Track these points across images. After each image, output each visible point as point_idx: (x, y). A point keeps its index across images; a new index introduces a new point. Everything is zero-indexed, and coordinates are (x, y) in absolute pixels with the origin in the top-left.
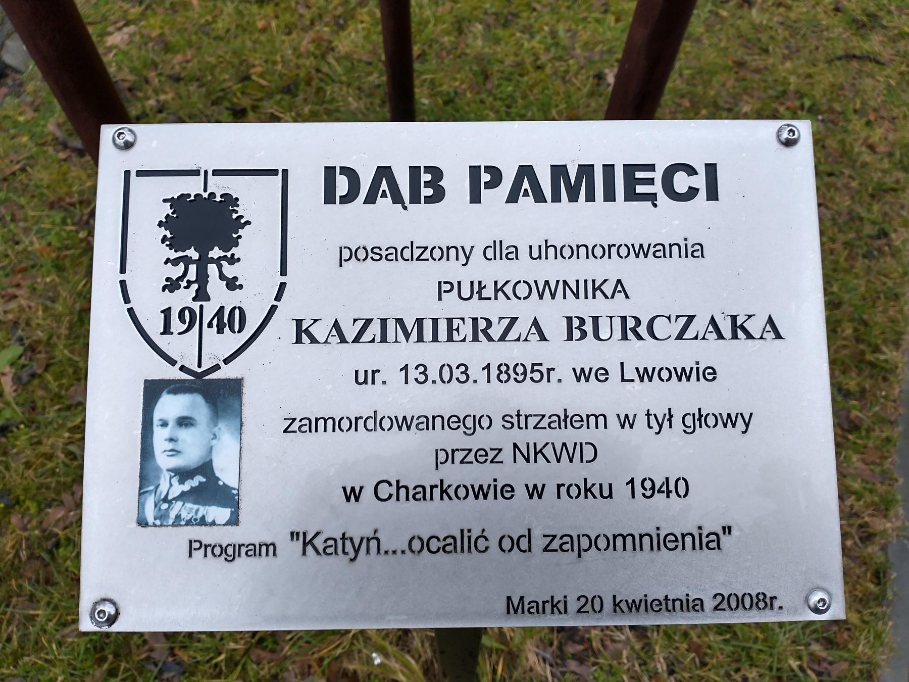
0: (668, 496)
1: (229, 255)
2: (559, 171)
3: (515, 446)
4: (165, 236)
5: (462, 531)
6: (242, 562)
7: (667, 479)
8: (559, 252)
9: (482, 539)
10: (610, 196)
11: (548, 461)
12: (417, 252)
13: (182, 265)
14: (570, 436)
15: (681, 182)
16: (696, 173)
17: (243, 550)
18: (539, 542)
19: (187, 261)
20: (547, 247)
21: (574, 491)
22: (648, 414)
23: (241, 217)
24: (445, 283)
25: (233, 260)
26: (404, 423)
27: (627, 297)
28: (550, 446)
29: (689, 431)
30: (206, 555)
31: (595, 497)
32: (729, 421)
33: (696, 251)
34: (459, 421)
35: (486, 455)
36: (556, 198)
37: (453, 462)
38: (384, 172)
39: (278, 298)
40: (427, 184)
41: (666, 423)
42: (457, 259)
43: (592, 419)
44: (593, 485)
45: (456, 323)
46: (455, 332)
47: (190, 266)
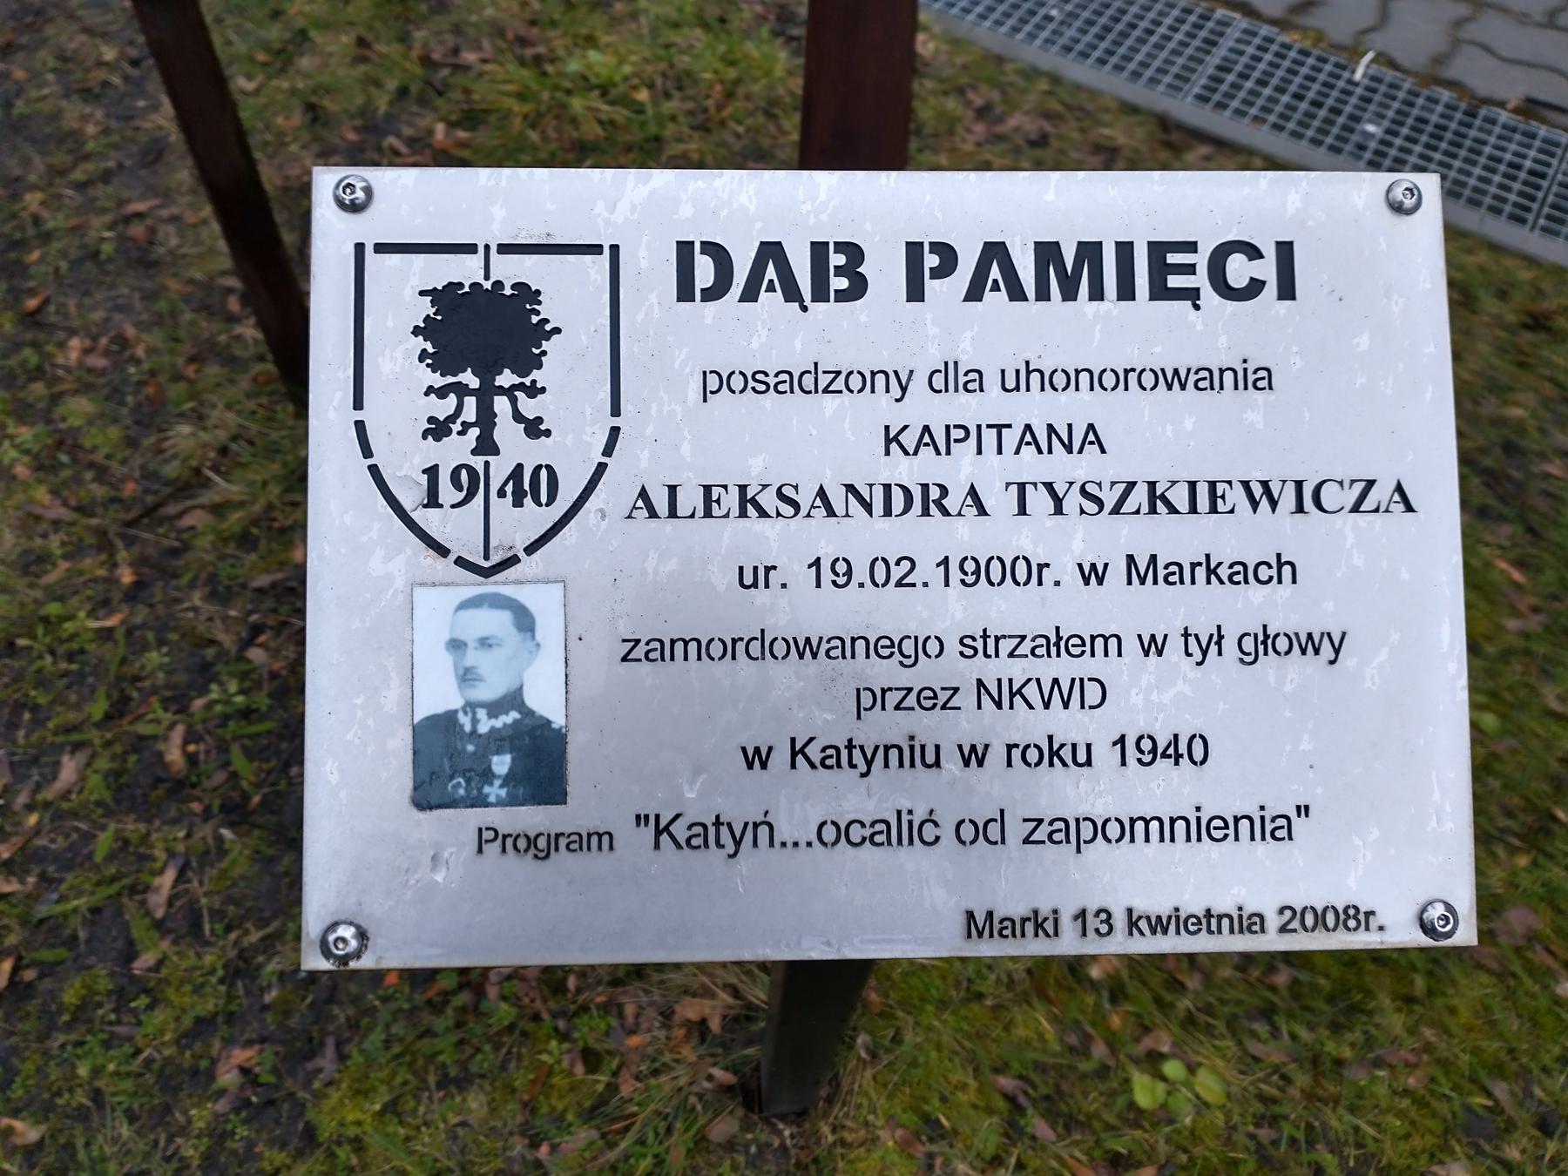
0: (1177, 763)
1: (527, 381)
2: (1047, 253)
3: (980, 683)
4: (424, 351)
5: (899, 813)
6: (562, 858)
7: (1176, 736)
8: (1048, 382)
9: (928, 826)
10: (1126, 292)
11: (1031, 707)
12: (824, 380)
13: (452, 399)
14: (1063, 668)
15: (1238, 270)
16: (1261, 256)
17: (563, 842)
18: (1016, 831)
19: (461, 390)
20: (1029, 373)
21: (1033, 755)
22: (1186, 635)
23: (546, 321)
24: (956, 427)
25: (534, 391)
26: (807, 648)
27: (1103, 451)
28: (1033, 684)
29: (1249, 659)
30: (504, 850)
31: (1065, 764)
32: (1309, 644)
33: (1258, 379)
34: (892, 646)
35: (935, 697)
36: (1043, 294)
37: (883, 708)
38: (771, 252)
39: (608, 451)
40: (839, 271)
41: (1213, 648)
42: (888, 391)
43: (1099, 642)
44: (1062, 746)
45: (1220, 489)
46: (1219, 501)
47: (467, 399)
